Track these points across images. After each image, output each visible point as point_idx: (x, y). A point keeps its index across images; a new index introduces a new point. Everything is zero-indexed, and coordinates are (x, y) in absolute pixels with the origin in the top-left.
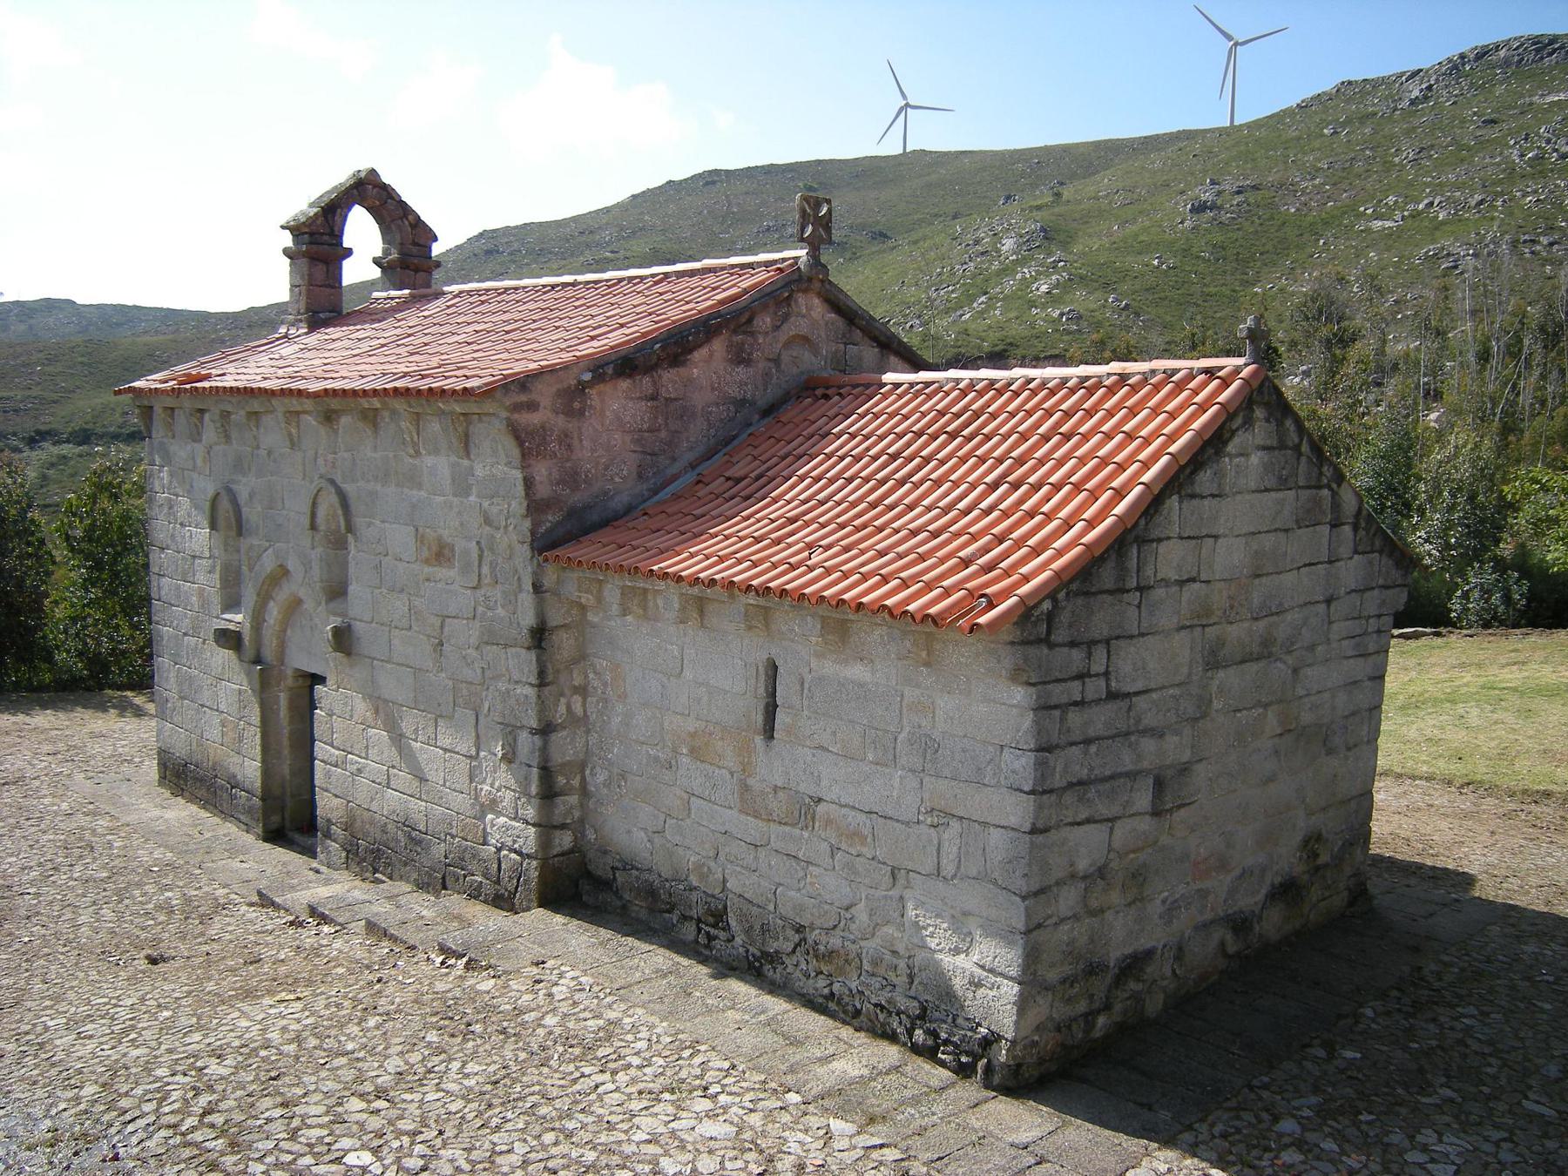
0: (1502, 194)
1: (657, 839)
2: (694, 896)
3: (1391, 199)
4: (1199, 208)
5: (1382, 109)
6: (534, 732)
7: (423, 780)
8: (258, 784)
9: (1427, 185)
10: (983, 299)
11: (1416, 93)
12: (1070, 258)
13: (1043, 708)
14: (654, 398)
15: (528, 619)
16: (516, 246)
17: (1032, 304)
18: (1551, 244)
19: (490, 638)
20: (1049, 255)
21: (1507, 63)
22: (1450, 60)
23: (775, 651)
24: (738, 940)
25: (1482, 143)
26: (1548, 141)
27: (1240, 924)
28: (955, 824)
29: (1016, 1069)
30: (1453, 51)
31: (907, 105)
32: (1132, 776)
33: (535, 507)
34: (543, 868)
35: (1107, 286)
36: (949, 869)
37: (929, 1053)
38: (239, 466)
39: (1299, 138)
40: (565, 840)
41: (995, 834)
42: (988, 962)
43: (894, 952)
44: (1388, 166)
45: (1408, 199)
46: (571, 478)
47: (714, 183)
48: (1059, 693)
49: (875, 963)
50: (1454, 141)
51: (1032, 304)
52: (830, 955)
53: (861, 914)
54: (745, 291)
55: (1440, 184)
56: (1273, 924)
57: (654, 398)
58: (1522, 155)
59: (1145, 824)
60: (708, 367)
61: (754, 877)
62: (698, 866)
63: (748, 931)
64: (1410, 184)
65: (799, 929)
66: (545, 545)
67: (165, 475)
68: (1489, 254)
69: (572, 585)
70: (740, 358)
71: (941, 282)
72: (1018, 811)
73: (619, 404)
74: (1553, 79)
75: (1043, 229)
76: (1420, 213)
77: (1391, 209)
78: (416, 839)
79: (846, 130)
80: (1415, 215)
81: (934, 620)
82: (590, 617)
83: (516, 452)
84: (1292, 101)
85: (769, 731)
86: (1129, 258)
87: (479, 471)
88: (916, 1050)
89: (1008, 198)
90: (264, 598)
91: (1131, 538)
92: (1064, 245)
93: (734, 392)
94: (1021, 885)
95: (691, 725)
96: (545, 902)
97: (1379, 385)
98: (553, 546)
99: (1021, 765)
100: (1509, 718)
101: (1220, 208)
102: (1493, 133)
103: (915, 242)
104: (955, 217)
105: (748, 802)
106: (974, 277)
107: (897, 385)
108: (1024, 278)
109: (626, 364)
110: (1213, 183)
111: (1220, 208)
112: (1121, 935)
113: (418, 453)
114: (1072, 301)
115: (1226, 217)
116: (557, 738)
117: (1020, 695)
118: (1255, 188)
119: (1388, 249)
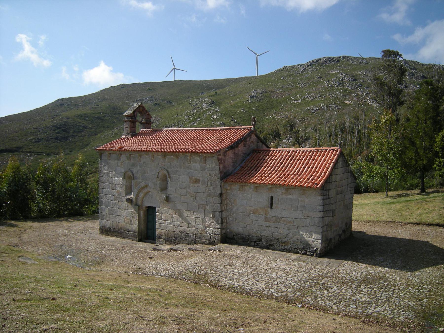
0: (324, 95)
1: (244, 229)
2: (254, 237)
3: (298, 95)
4: (252, 97)
5: (294, 73)
6: (219, 212)
7: (189, 224)
8: (137, 230)
9: (307, 92)
10: (199, 119)
11: (302, 70)
12: (221, 109)
13: (324, 199)
14: (234, 153)
15: (219, 192)
16: (69, 103)
17: (212, 121)
18: (336, 107)
19: (209, 196)
20: (215, 108)
21: (323, 63)
22: (310, 62)
23: (273, 195)
24: (264, 243)
25: (319, 83)
26: (334, 82)
27: (340, 236)
28: (309, 218)
29: (320, 254)
30: (311, 60)
31: (175, 68)
32: (330, 210)
33: (221, 172)
34: (221, 237)
35: (230, 116)
36: (308, 225)
37: (305, 254)
38: (133, 165)
39: (275, 80)
40: (224, 231)
41: (316, 218)
42: (315, 238)
43: (298, 240)
44: (297, 87)
45: (302, 96)
46: (224, 167)
47: (124, 87)
48: (325, 197)
49: (294, 242)
50: (312, 82)
51: (212, 121)
52: (285, 242)
53: (291, 235)
54: (245, 134)
55: (310, 92)
56: (343, 237)
57: (234, 153)
58: (328, 86)
59: (331, 218)
60: (241, 148)
61: (268, 232)
62: (255, 232)
63: (267, 241)
64: (302, 92)
65: (278, 239)
66: (222, 179)
67: (106, 167)
68: (322, 109)
69: (227, 186)
70: (245, 146)
71: (188, 115)
72: (320, 215)
73: (230, 154)
74: (334, 67)
75: (213, 102)
76: (305, 99)
77: (298, 98)
78: (186, 235)
79: (159, 74)
80: (304, 99)
81: (310, 187)
82: (228, 191)
83: (218, 163)
84: (273, 71)
85: (271, 207)
86: (236, 109)
87: (208, 166)
88: (303, 254)
89: (202, 93)
90: (139, 191)
91: (330, 175)
92: (219, 106)
93: (244, 152)
94: (321, 225)
95: (253, 208)
96: (222, 242)
97: (305, 142)
98: (223, 179)
99: (320, 208)
100: (359, 209)
101: (257, 97)
102: (321, 80)
103: (180, 104)
104: (189, 98)
105: (266, 219)
106: (196, 114)
107: (274, 151)
108: (209, 114)
109: (232, 147)
110: (255, 91)
111: (257, 97)
112: (331, 235)
113: (190, 163)
114: (222, 121)
115: (259, 99)
116: (223, 213)
117: (320, 198)
118: (265, 92)
119: (298, 108)
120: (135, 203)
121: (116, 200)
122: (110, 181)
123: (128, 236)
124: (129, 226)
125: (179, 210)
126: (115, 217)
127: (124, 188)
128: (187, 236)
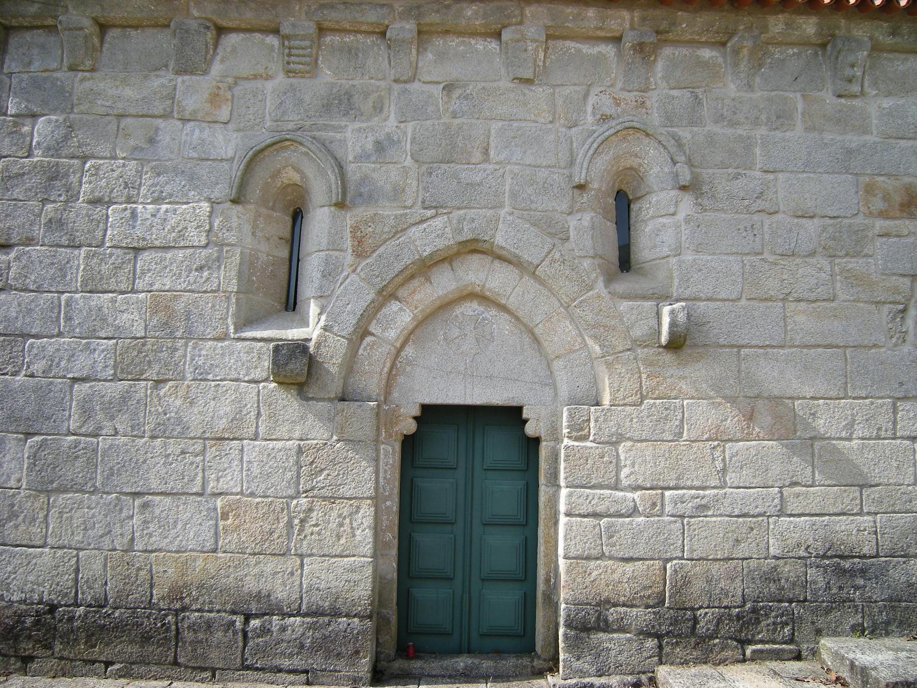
120: (335, 388)
121: (125, 370)
122: (81, 224)
123: (262, 651)
124: (270, 565)
125: (777, 400)
126: (118, 505)
127: (227, 277)
128: (851, 573)
